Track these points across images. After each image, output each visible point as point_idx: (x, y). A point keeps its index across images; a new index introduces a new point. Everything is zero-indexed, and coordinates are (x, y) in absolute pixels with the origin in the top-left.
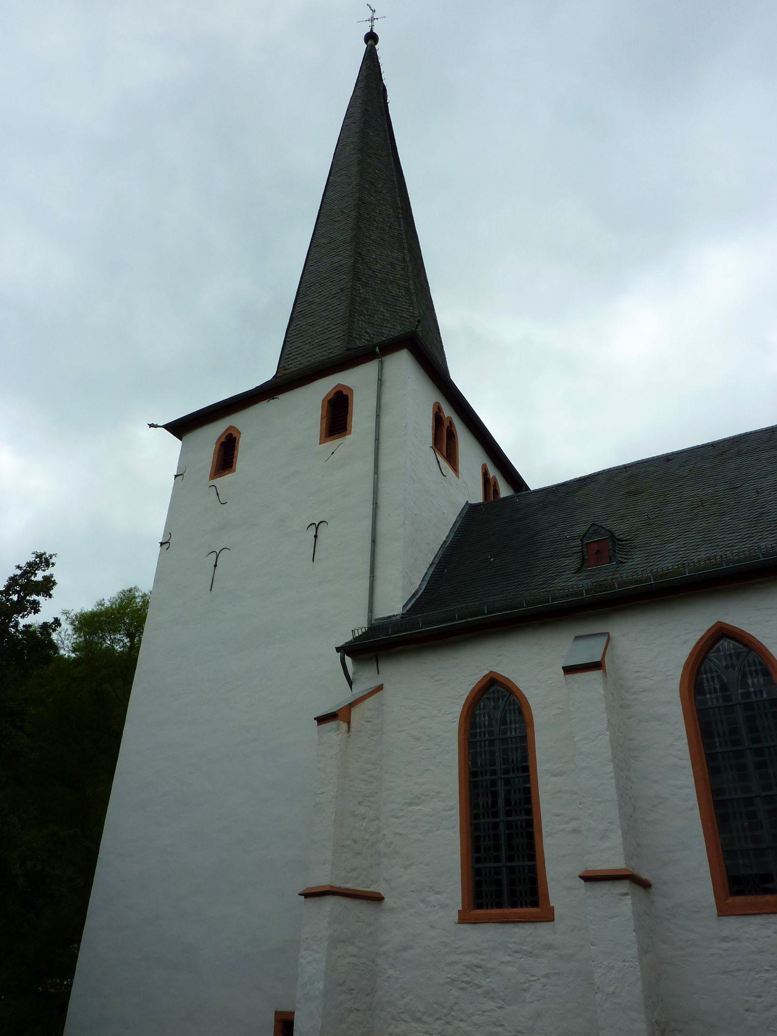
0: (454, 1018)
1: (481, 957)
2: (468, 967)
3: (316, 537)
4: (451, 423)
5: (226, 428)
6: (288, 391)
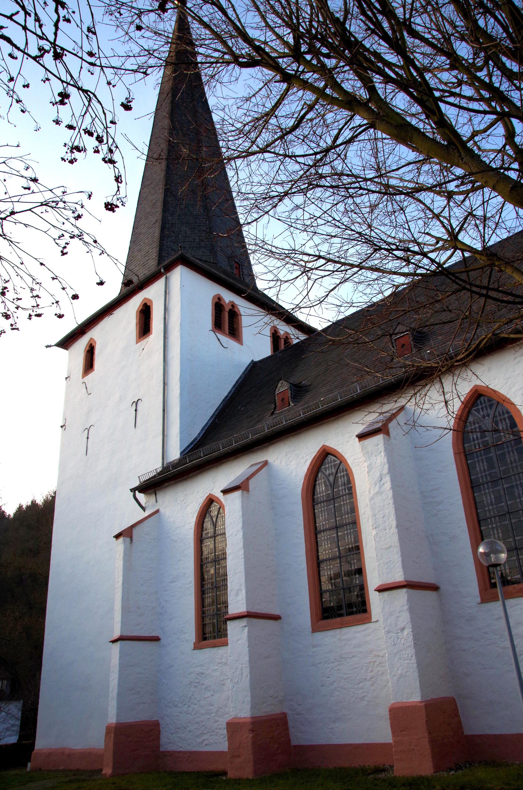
0: (192, 703)
1: (204, 668)
2: (198, 674)
3: (136, 410)
4: (233, 305)
5: (89, 340)
6: (194, 270)
